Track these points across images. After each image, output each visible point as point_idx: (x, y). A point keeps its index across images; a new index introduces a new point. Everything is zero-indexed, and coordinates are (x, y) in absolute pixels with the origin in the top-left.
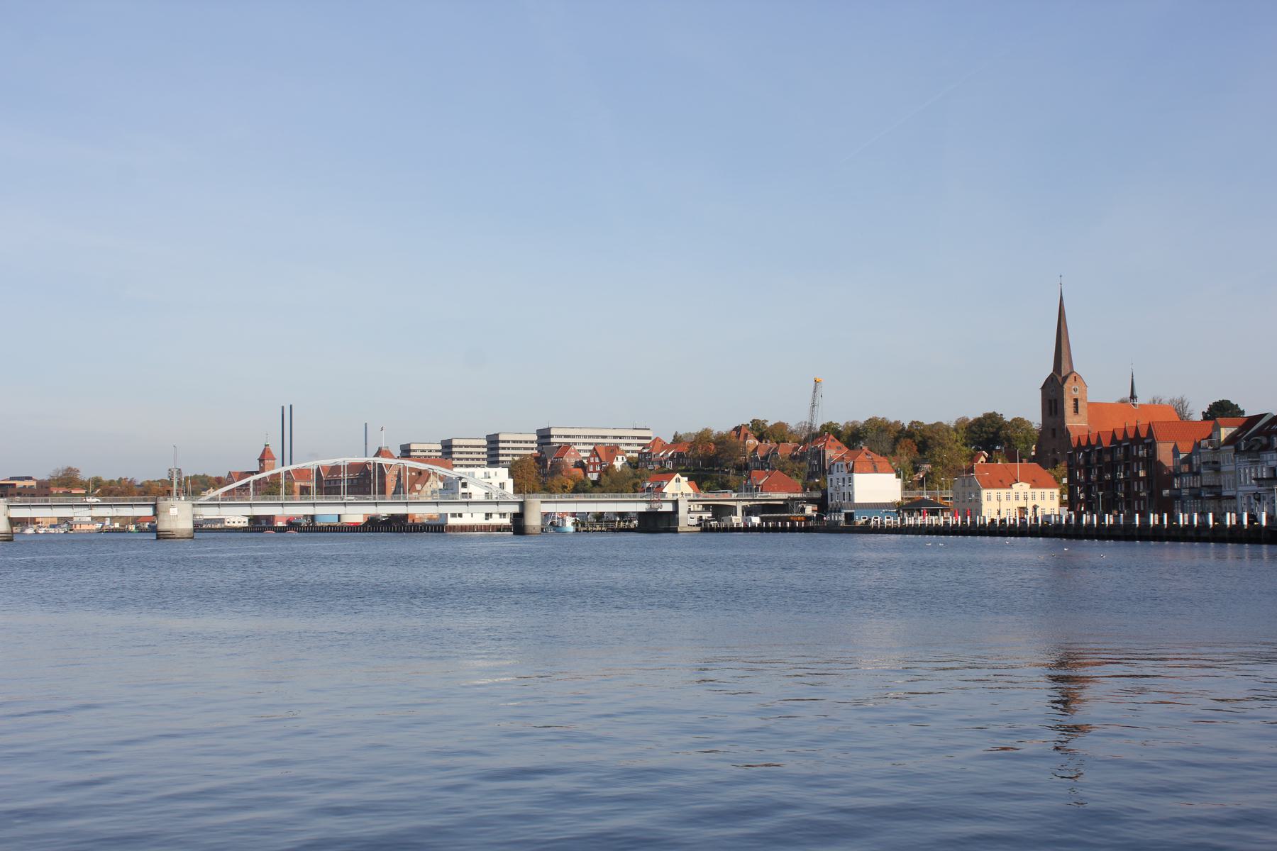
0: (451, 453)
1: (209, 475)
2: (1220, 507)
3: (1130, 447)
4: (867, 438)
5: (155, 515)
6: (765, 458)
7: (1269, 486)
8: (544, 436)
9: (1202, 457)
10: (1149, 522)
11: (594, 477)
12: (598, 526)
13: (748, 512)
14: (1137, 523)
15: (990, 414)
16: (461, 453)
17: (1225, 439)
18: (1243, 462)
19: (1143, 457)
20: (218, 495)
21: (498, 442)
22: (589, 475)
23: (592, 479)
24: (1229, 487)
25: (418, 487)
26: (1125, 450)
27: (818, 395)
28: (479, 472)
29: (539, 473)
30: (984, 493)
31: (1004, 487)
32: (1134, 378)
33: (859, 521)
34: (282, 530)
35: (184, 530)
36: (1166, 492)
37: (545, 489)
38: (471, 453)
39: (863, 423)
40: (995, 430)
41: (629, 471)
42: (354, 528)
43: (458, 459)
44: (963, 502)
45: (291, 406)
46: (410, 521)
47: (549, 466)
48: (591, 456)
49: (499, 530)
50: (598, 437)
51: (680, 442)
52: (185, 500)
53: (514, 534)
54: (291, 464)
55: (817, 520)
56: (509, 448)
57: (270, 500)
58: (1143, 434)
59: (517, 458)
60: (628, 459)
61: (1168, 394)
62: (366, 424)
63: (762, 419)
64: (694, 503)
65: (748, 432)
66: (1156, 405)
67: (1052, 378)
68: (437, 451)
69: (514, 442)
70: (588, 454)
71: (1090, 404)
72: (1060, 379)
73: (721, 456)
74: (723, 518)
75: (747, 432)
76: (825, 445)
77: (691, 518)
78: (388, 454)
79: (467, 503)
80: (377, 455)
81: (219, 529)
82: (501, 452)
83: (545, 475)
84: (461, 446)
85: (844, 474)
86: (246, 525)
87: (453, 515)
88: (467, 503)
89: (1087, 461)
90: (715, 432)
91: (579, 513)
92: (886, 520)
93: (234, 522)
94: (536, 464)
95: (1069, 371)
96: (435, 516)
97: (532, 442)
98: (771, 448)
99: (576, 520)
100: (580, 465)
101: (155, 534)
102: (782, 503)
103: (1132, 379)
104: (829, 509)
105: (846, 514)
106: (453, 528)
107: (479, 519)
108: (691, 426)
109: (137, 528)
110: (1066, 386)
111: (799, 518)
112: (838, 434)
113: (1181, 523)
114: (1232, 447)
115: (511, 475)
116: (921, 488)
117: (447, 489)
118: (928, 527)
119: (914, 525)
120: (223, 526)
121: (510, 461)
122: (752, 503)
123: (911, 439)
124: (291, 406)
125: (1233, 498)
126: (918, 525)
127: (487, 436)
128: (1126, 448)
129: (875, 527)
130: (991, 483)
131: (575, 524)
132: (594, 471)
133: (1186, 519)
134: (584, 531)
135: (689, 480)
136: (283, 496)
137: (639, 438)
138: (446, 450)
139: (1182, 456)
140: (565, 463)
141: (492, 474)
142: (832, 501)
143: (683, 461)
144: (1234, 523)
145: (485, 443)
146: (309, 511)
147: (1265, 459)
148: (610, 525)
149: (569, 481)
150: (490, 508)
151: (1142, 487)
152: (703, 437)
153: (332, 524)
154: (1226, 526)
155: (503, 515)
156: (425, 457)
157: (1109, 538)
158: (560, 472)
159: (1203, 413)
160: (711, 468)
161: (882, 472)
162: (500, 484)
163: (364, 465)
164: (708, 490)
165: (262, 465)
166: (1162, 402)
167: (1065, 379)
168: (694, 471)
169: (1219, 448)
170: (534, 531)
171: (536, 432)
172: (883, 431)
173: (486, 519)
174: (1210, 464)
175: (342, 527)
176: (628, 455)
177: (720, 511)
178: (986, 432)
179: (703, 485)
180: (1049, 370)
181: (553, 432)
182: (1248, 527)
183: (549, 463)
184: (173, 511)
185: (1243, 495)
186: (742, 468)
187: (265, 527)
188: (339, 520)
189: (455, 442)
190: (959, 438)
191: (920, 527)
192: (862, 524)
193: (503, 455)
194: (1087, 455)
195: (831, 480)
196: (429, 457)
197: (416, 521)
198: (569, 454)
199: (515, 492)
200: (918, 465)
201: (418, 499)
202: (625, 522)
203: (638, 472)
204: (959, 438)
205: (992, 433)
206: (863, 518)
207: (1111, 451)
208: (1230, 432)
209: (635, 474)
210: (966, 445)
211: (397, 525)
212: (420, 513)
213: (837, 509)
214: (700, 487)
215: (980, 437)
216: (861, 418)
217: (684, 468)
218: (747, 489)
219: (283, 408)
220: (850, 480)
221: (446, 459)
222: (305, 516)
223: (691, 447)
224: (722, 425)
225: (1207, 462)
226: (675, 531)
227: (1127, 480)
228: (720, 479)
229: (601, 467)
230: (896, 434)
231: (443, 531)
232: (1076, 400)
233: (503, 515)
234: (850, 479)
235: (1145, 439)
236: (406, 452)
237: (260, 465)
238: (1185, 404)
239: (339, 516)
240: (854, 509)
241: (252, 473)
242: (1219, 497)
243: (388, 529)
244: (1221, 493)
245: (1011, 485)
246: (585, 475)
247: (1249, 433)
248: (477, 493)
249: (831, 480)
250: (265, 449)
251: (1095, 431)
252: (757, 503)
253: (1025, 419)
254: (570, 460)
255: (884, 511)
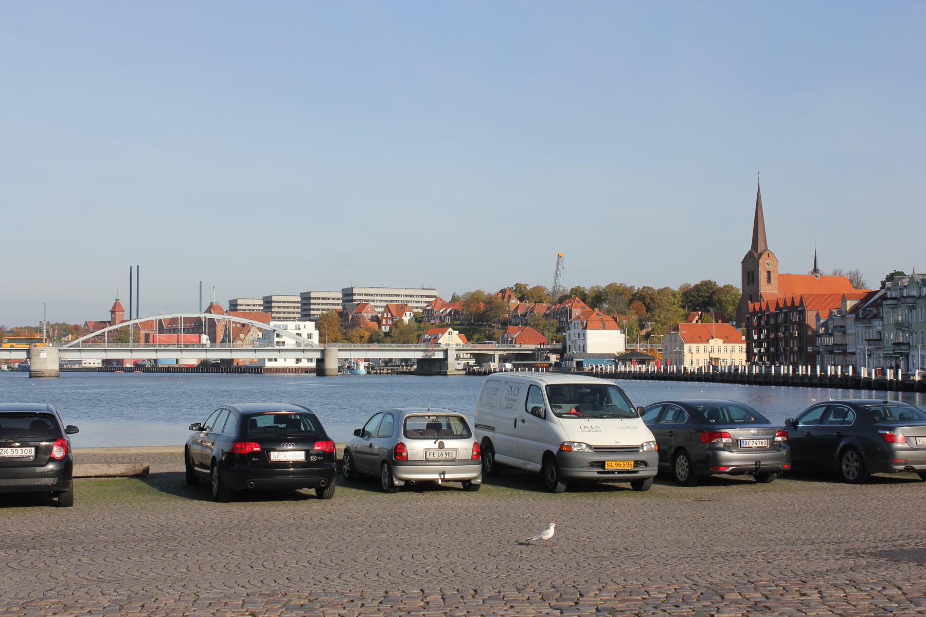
0: (271, 307)
1: (68, 323)
2: (846, 360)
3: (788, 313)
4: (607, 299)
5: (28, 357)
6: (524, 315)
7: (875, 345)
8: (348, 295)
9: (835, 323)
10: (780, 371)
11: (386, 329)
12: (385, 369)
13: (504, 359)
14: (773, 372)
15: (706, 282)
16: (279, 307)
17: (850, 309)
18: (861, 328)
19: (796, 322)
20: (79, 343)
21: (310, 298)
22: (383, 327)
23: (385, 331)
24: (852, 345)
25: (242, 336)
26: (785, 314)
27: (560, 267)
28: (291, 325)
29: (342, 325)
30: (687, 346)
31: (702, 342)
32: (817, 255)
33: (587, 368)
34: (130, 370)
35: (52, 370)
36: (810, 349)
37: (346, 339)
38: (288, 307)
39: (604, 287)
40: (709, 294)
41: (415, 324)
42: (190, 369)
43: (277, 313)
44: (671, 353)
45: (138, 266)
46: (235, 364)
47: (350, 320)
48: (385, 311)
49: (306, 372)
50: (392, 295)
51: (457, 301)
52: (52, 347)
53: (317, 375)
54: (138, 318)
55: (555, 366)
56: (319, 304)
57: (121, 347)
58: (797, 303)
59: (324, 312)
60: (415, 314)
61: (847, 267)
62: (201, 282)
63: (523, 283)
64: (463, 352)
65: (512, 294)
66: (837, 276)
67: (750, 255)
68: (259, 305)
69: (323, 299)
70: (382, 310)
71: (780, 276)
72: (756, 255)
73: (488, 313)
74: (483, 364)
75: (510, 293)
76: (572, 305)
77: (458, 364)
78: (220, 311)
79: (279, 351)
80: (208, 311)
81: (78, 369)
82: (312, 307)
83: (346, 327)
84: (279, 302)
85: (580, 330)
86: (100, 366)
87: (270, 360)
88: (279, 351)
89: (759, 323)
90: (486, 293)
91: (372, 359)
92: (609, 367)
93: (90, 363)
94: (339, 318)
95: (763, 249)
96: (256, 360)
97: (338, 299)
98: (529, 307)
99: (369, 364)
100: (376, 319)
101: (29, 373)
102: (530, 352)
103: (815, 256)
104: (564, 358)
105: (577, 362)
106: (270, 370)
107: (291, 363)
108: (464, 288)
109: (8, 367)
110: (761, 261)
111: (542, 365)
112: (583, 297)
113: (829, 373)
114: (854, 315)
115: (317, 327)
116: (645, 341)
117: (265, 338)
118: (634, 373)
119: (634, 371)
120: (81, 366)
121: (320, 315)
122: (507, 352)
123: (641, 301)
124: (138, 266)
125: (854, 354)
126: (915, 380)
127: (301, 294)
128: (786, 313)
129: (597, 372)
130: (692, 339)
131: (367, 368)
132: (387, 324)
133: (804, 370)
134: (374, 373)
135: (459, 333)
136: (131, 343)
137: (426, 296)
138: (267, 305)
139: (822, 321)
140: (363, 318)
141: (302, 327)
142: (569, 351)
143: (458, 317)
144: (758, 371)
145: (299, 299)
146: (152, 355)
147: (874, 325)
148: (395, 368)
149: (366, 332)
150: (299, 355)
151: (795, 345)
152: (474, 298)
153: (171, 366)
154: (781, 374)
155: (310, 360)
156: (250, 310)
157: (756, 383)
158: (359, 325)
159: (882, 282)
160: (481, 323)
161: (610, 329)
162: (308, 335)
163: (199, 319)
164: (478, 341)
165: (113, 316)
166: (841, 274)
167: (760, 255)
168: (467, 325)
169: (845, 316)
170: (332, 373)
171: (299, 295)
172: (621, 294)
173: (297, 363)
174: (839, 328)
175: (180, 368)
176: (415, 310)
177: (481, 359)
178: (702, 296)
179: (474, 337)
180: (748, 248)
181: (355, 291)
182: (841, 376)
183: (350, 317)
184: (43, 355)
185: (860, 352)
186: (505, 324)
187: (115, 368)
188: (177, 363)
189: (274, 299)
190: (676, 301)
191: (624, 373)
192: (589, 370)
193: (314, 310)
194: (760, 318)
195: (569, 334)
196: (253, 310)
197: (240, 364)
198: (367, 310)
199: (320, 341)
200: (644, 323)
201: (242, 347)
202: (407, 366)
203: (422, 326)
204: (676, 301)
205: (707, 297)
206: (590, 366)
207: (776, 316)
208: (854, 304)
209: (419, 327)
210: (683, 307)
211: (226, 367)
212: (243, 357)
213: (570, 358)
214: (469, 339)
215: (697, 300)
216: (603, 284)
217: (459, 322)
218: (504, 341)
219: (131, 267)
220: (584, 335)
221: (267, 312)
222: (149, 360)
223: (464, 305)
224: (491, 288)
225: (837, 326)
226: (445, 374)
227: (786, 339)
228: (487, 332)
229: (392, 320)
230: (631, 297)
231: (261, 373)
232: (769, 272)
233: (310, 360)
234: (584, 334)
235: (798, 307)
236: (234, 306)
237: (112, 316)
238: (860, 276)
239: (177, 360)
240: (584, 358)
241: (103, 324)
242: (845, 353)
243: (217, 370)
244: (846, 349)
245: (708, 341)
246: (380, 327)
247: (865, 305)
248: (290, 343)
249: (569, 334)
250: (116, 302)
251: (781, 297)
252: (511, 352)
253: (734, 286)
254: (367, 315)
255: (607, 360)
